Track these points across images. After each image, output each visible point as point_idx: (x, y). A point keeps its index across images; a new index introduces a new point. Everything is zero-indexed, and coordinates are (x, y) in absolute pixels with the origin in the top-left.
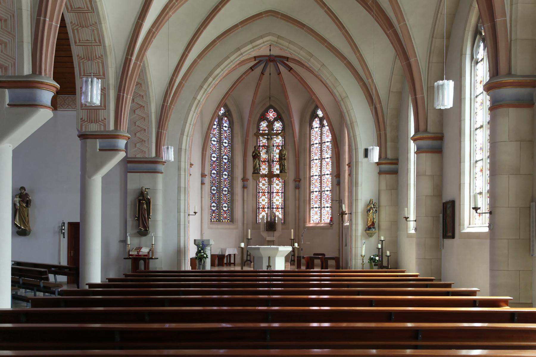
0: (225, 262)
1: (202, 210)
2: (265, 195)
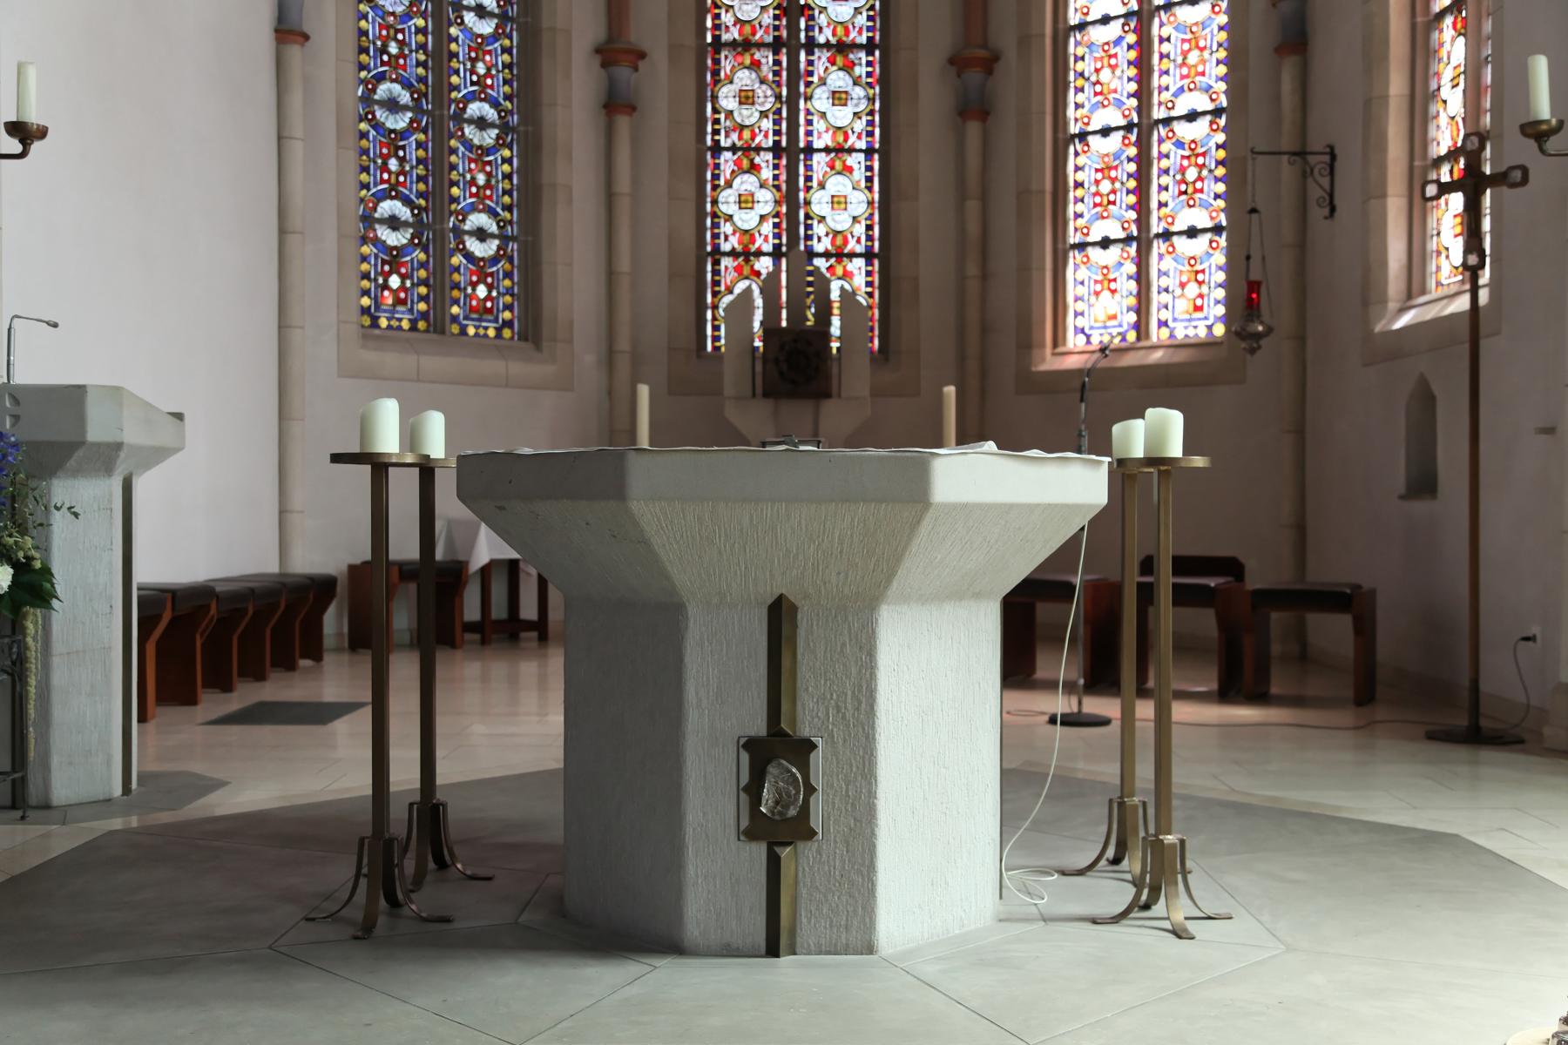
0: (471, 610)
1: (283, 231)
2: (754, 168)
